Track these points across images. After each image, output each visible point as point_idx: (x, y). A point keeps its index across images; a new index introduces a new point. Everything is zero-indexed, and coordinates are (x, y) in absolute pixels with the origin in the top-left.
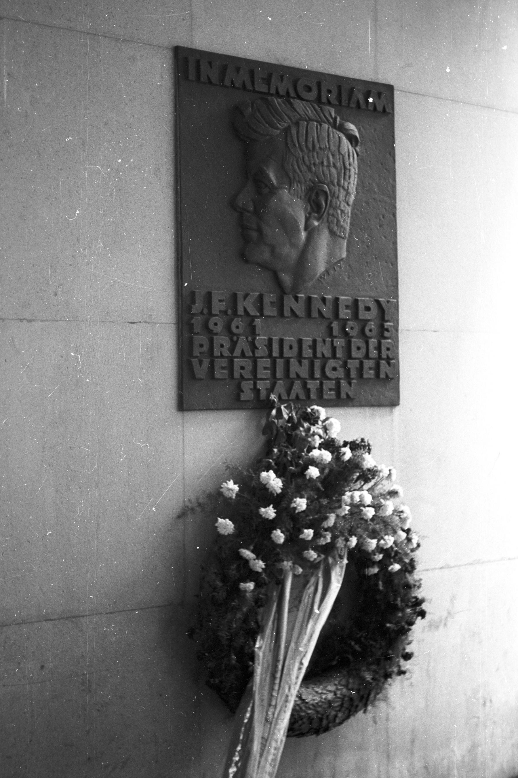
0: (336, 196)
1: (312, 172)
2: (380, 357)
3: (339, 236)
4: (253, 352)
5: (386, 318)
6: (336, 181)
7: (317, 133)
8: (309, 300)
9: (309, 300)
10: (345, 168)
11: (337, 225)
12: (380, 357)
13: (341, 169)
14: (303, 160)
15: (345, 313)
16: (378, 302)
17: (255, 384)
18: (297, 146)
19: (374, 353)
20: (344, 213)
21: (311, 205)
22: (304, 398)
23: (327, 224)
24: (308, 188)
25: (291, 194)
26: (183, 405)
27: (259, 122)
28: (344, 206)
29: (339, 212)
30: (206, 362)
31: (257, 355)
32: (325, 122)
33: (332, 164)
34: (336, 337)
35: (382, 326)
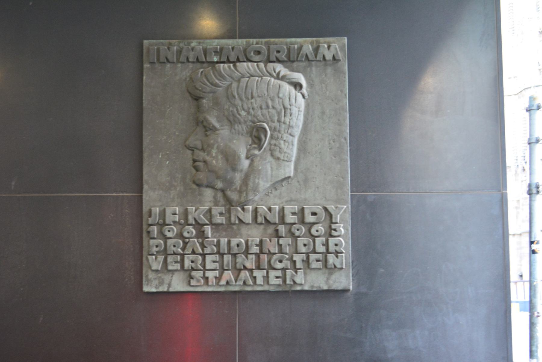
0: (278, 130)
1: (251, 115)
2: (328, 252)
3: (284, 160)
4: (203, 250)
5: (334, 221)
6: (276, 118)
7: (257, 85)
8: (256, 211)
9: (256, 211)
10: (285, 108)
11: (280, 152)
12: (328, 252)
13: (281, 110)
14: (242, 107)
15: (290, 218)
16: (326, 209)
17: (204, 274)
18: (237, 97)
19: (321, 249)
20: (288, 142)
21: (252, 139)
22: (252, 284)
23: (270, 152)
24: (249, 127)
25: (232, 133)
26: (521, 310)
27: (216, 86)
28: (287, 137)
29: (282, 142)
30: (161, 258)
31: (205, 252)
32: (267, 76)
33: (271, 107)
34: (282, 237)
35: (330, 227)
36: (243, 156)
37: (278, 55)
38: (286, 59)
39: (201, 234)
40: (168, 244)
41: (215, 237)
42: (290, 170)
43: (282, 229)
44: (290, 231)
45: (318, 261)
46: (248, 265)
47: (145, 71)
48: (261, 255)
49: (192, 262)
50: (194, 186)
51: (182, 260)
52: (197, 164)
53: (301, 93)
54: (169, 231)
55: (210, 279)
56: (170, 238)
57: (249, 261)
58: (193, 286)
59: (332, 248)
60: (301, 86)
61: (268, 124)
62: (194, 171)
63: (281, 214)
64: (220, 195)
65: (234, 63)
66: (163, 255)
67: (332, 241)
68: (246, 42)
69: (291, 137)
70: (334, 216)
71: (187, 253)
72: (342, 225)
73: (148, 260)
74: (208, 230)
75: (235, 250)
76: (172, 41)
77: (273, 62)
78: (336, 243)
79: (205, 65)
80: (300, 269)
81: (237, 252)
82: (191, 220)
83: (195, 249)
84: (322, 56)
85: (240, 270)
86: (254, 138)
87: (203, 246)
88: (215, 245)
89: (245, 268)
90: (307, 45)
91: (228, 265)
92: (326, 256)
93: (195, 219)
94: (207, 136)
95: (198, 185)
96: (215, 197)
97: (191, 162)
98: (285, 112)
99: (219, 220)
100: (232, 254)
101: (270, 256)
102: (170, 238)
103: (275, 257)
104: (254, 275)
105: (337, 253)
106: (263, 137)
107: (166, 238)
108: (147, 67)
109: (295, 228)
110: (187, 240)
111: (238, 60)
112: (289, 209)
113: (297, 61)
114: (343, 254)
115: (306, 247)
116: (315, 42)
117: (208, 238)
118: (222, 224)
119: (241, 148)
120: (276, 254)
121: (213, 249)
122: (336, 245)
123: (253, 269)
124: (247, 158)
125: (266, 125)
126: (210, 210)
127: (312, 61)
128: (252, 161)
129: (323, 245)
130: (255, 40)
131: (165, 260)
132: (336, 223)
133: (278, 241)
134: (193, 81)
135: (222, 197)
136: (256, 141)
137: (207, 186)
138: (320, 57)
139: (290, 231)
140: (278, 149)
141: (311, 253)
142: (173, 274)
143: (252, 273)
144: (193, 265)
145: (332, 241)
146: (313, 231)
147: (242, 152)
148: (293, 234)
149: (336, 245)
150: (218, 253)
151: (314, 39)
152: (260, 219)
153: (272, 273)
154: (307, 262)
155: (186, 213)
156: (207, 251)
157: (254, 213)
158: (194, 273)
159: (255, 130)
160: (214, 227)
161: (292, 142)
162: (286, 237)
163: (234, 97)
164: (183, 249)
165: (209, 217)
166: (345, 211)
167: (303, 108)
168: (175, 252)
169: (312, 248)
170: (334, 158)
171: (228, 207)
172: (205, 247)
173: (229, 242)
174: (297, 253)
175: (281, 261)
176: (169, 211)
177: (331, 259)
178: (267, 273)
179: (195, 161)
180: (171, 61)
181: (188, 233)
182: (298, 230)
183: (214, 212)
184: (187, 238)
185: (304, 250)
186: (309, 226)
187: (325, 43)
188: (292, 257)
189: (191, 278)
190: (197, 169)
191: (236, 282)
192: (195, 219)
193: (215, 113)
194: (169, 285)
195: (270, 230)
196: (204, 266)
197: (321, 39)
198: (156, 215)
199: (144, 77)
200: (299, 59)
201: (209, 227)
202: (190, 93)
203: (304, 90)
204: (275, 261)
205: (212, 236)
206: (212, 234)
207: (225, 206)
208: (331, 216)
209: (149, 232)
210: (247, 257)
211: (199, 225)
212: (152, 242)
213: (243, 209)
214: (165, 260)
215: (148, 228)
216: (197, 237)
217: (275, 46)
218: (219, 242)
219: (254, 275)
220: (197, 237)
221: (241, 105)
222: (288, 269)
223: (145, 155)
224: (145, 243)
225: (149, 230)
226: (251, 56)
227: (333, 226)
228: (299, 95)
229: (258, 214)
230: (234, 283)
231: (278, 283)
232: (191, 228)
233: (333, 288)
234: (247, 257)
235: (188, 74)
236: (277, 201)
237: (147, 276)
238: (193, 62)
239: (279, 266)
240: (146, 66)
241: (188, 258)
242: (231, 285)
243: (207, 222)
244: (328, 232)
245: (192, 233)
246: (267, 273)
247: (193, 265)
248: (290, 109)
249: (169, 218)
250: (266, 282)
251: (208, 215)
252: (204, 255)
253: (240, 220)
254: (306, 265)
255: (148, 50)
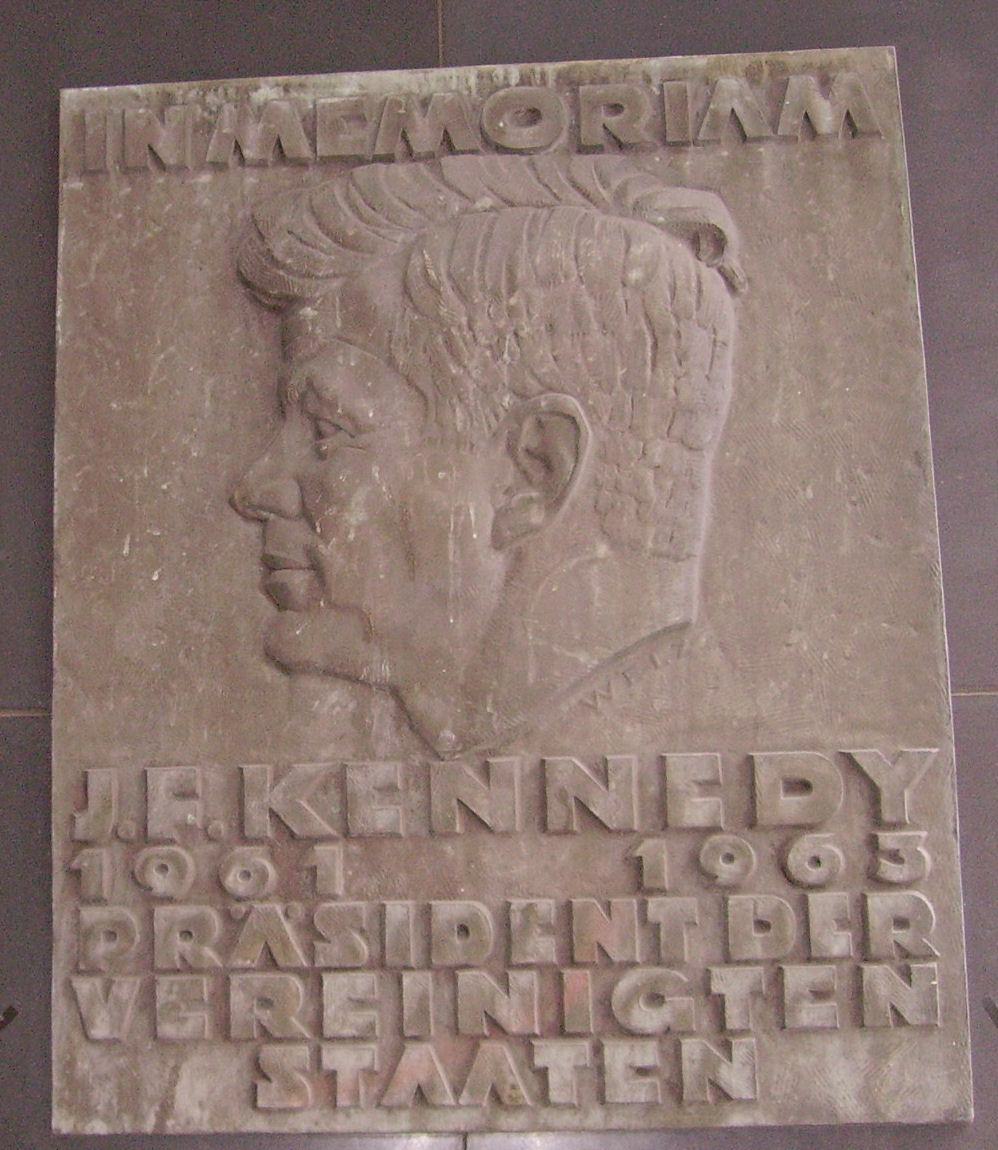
15: (697, 810)
16: (850, 763)
30: (128, 989)
35: (873, 843)
36: (481, 536)
37: (613, 121)
38: (647, 137)
39: (302, 884)
40: (159, 925)
41: (361, 896)
42: (680, 595)
43: (662, 855)
44: (694, 861)
45: (820, 994)
46: (510, 1014)
47: (64, 207)
48: (567, 973)
49: (265, 1003)
50: (269, 673)
51: (222, 995)
52: (281, 576)
53: (721, 271)
54: (163, 868)
55: (341, 1079)
56: (169, 900)
57: (515, 998)
58: (268, 1111)
59: (885, 936)
60: (719, 242)
61: (583, 396)
62: (265, 607)
63: (653, 790)
64: (381, 710)
65: (430, 158)
66: (136, 974)
67: (880, 904)
68: (480, 76)
69: (686, 454)
70: (885, 795)
71: (239, 963)
72: (924, 834)
73: (72, 995)
74: (332, 859)
75: (455, 949)
76: (170, 87)
77: (596, 149)
78: (903, 913)
79: (312, 174)
80: (743, 1032)
81: (463, 960)
82: (259, 822)
83: (276, 950)
84: (798, 121)
85: (475, 1041)
86: (526, 462)
87: (311, 932)
88: (362, 931)
89: (497, 1027)
90: (731, 81)
91: (423, 1011)
92: (858, 971)
93: (273, 814)
94: (321, 456)
95: (285, 668)
96: (358, 719)
97: (257, 569)
98: (655, 345)
99: (382, 816)
100: (437, 970)
101: (608, 975)
102: (169, 900)
103: (626, 984)
104: (539, 1062)
105: (906, 961)
106: (565, 451)
107: (150, 899)
108: (72, 192)
109: (715, 848)
110: (243, 908)
111: (448, 145)
112: (687, 766)
113: (695, 143)
114: (934, 965)
115: (770, 934)
116: (766, 68)
117: (334, 897)
118: (394, 836)
119: (474, 499)
120: (632, 964)
121: (354, 952)
122: (901, 923)
123: (535, 1036)
124: (497, 542)
125: (573, 404)
126: (340, 779)
127: (759, 140)
128: (519, 557)
129: (843, 924)
130: (515, 71)
131: (149, 992)
132: (897, 825)
133: (643, 905)
134: (261, 236)
135: (389, 721)
136: (538, 475)
137: (330, 673)
138: (790, 122)
139: (694, 861)
140: (632, 507)
141: (792, 959)
142: (182, 1057)
143: (530, 1055)
144: (265, 1016)
145: (880, 904)
146: (797, 859)
147: (479, 513)
148: (708, 879)
149: (901, 923)
150: (379, 964)
151: (764, 56)
152: (556, 814)
153: (619, 1056)
154: (774, 997)
155: (238, 789)
156: (330, 952)
157: (533, 785)
158: (271, 1053)
159: (528, 425)
160: (355, 848)
161: (690, 472)
162: (676, 892)
163: (435, 288)
164: (227, 947)
165: (335, 810)
166: (933, 773)
167: (730, 330)
168: (190, 960)
169: (792, 930)
170: (873, 541)
171: (417, 759)
172: (321, 937)
173: (426, 913)
174: (727, 960)
175: (656, 999)
176: (162, 781)
177: (880, 978)
178: (598, 1050)
179: (270, 565)
180: (170, 160)
181: (246, 875)
182: (729, 858)
183: (357, 780)
184: (239, 900)
185: (756, 945)
186: (776, 838)
187: (806, 68)
188: (707, 977)
189: (259, 1071)
190: (279, 597)
191: (457, 1092)
192: (273, 814)
193: (352, 357)
194: (166, 1108)
195: (608, 864)
196: (318, 1026)
197: (793, 57)
198: (628, 779)
199: (62, 233)
200: (701, 136)
201: (337, 849)
202: (247, 284)
203: (732, 260)
204: (634, 993)
205: (347, 889)
206: (349, 882)
207: (404, 757)
208: (874, 794)
209: (75, 875)
210: (504, 982)
211: (290, 840)
212: (91, 915)
213: (486, 770)
214: (149, 992)
215: (74, 855)
216: (286, 893)
217: (600, 90)
218: (381, 913)
219: (539, 1062)
220: (286, 893)
221: (464, 320)
222: (691, 1034)
223: (64, 544)
224: (62, 923)
225: (75, 864)
226: (502, 132)
227: (888, 840)
228: (710, 275)
229: (551, 792)
230: (450, 1100)
231: (642, 1096)
232: (260, 858)
233: (892, 1116)
234: (504, 982)
235: (248, 213)
236: (632, 732)
237: (70, 1065)
238: (261, 164)
239: (646, 1018)
240: (72, 185)
241: (243, 987)
242: (435, 1107)
243: (329, 830)
244: (861, 866)
245: (264, 876)
246: (598, 1050)
247: (265, 1016)
248: (678, 335)
249: (164, 813)
250: (590, 1093)
251: (334, 794)
252: (315, 978)
253: (472, 817)
254: (771, 1015)
255: (80, 124)
